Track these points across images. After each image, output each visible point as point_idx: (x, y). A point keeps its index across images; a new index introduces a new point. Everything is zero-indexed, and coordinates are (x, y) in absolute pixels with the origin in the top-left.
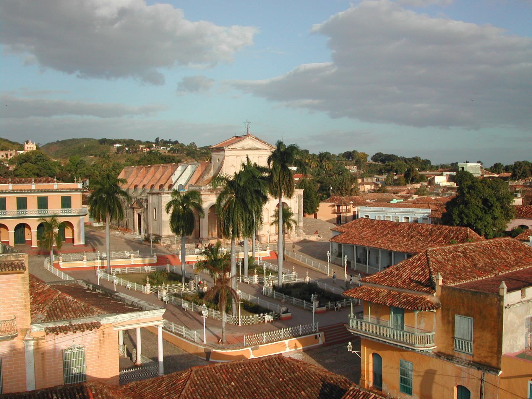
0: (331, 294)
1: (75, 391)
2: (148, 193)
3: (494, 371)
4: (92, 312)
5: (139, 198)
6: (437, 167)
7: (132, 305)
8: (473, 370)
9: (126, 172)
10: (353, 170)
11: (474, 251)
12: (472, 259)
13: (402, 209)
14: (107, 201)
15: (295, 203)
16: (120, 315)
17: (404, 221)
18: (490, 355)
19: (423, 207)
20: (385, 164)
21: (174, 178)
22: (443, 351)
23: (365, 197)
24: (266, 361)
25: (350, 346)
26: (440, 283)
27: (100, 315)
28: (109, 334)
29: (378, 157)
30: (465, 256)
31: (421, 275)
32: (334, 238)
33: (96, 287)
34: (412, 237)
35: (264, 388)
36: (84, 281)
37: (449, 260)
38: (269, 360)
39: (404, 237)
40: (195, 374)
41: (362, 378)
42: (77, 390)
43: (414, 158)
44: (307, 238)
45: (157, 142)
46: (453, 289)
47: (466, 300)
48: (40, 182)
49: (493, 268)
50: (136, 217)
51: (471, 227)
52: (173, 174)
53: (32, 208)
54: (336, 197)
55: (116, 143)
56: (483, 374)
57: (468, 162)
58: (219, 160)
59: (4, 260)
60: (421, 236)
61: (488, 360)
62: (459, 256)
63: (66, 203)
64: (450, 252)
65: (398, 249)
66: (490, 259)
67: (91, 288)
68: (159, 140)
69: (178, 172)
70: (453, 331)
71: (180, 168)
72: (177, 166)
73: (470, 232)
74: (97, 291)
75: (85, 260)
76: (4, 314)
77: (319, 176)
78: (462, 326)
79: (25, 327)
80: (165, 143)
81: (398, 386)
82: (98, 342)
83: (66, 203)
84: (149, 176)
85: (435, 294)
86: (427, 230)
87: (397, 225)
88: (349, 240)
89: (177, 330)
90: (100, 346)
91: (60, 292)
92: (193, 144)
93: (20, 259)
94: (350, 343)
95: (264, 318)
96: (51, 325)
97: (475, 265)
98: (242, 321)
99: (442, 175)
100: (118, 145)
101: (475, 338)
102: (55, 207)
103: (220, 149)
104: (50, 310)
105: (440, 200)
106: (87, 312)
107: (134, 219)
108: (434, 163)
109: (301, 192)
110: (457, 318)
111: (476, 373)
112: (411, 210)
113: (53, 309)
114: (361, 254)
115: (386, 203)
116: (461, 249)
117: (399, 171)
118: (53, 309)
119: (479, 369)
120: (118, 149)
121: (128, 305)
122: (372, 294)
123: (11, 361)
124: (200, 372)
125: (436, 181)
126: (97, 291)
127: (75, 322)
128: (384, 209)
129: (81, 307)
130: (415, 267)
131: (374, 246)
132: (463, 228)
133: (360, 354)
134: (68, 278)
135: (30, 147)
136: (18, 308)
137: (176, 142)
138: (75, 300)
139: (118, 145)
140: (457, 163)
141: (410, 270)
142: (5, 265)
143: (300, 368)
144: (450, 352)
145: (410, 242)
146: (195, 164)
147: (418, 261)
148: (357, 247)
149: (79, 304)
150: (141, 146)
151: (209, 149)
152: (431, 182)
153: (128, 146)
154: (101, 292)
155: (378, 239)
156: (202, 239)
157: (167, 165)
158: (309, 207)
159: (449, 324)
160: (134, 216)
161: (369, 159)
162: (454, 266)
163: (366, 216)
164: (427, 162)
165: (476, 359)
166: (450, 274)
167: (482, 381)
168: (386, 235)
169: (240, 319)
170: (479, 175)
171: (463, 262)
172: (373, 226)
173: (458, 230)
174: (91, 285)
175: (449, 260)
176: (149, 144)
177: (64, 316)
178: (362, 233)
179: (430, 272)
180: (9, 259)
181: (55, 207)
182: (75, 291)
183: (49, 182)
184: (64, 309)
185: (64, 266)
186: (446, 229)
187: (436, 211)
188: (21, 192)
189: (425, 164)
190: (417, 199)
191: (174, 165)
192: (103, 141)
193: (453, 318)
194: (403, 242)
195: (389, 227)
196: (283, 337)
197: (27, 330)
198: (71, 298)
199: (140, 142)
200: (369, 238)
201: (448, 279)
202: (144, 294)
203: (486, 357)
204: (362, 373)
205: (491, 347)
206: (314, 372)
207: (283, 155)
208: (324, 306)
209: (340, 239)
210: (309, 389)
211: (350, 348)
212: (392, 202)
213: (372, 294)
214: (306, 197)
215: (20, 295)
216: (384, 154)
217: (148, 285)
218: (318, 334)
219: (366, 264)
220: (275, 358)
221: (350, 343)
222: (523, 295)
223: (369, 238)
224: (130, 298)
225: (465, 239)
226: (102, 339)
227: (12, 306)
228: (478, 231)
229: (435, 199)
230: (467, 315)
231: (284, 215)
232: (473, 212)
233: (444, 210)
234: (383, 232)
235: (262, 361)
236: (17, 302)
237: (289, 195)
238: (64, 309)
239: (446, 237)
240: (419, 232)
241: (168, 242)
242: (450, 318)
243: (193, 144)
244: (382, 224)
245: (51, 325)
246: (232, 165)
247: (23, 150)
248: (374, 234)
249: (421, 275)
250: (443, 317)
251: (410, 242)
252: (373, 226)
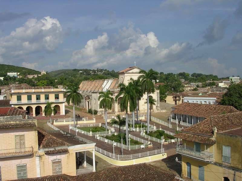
0: (170, 136)
1: (55, 178)
2: (92, 93)
3: (240, 170)
4: (64, 145)
5: (88, 94)
6: (220, 79)
7: (82, 141)
8: (231, 170)
9: (83, 83)
10: (183, 80)
11: (232, 117)
12: (231, 120)
13: (203, 98)
14: (74, 97)
15: (155, 96)
16: (76, 146)
17: (204, 103)
18: (238, 163)
19: (213, 97)
20: (197, 77)
21: (103, 86)
22: (218, 162)
23: (188, 93)
24: (138, 166)
25: (177, 159)
26: (216, 131)
27: (68, 146)
28: (72, 154)
29: (193, 75)
30: (228, 119)
31: (208, 128)
32: (172, 111)
33: (68, 133)
34: (207, 110)
35: (137, 178)
36: (63, 131)
37: (220, 121)
38: (140, 166)
39: (203, 110)
40: (107, 171)
41: (182, 173)
42: (56, 178)
43: (210, 75)
44: (161, 111)
45: (98, 70)
46: (222, 134)
47: (227, 139)
48: (46, 88)
49: (241, 125)
50: (87, 103)
51: (232, 105)
52: (103, 84)
53: (43, 99)
54: (174, 93)
55: (80, 71)
56: (235, 172)
57: (233, 76)
58: (122, 78)
59: (27, 122)
60: (211, 110)
61: (237, 166)
62: (226, 119)
63: (57, 97)
64: (221, 118)
65: (201, 116)
66: (239, 121)
67: (65, 134)
68: (99, 69)
69: (105, 83)
70: (222, 153)
71: (106, 81)
72: (105, 80)
73: (233, 108)
74: (68, 135)
75: (65, 121)
76: (27, 145)
77: (171, 84)
78: (226, 151)
79: (36, 151)
80: (101, 71)
81: (198, 176)
82: (67, 157)
83: (57, 97)
84: (93, 85)
85: (214, 136)
86: (213, 107)
87: (200, 105)
88: (179, 112)
89: (102, 152)
90: (68, 159)
91: (51, 136)
92: (113, 71)
93: (34, 122)
94: (177, 158)
95: (140, 147)
96: (47, 150)
97: (233, 123)
98: (130, 148)
99: (222, 82)
100: (81, 72)
101: (231, 156)
102: (52, 99)
103: (123, 73)
104: (47, 143)
105: (221, 94)
106: (62, 144)
107: (86, 104)
108: (219, 77)
109: (158, 91)
110: (224, 147)
111: (232, 172)
112: (207, 98)
113: (48, 143)
114: (184, 118)
115: (196, 95)
116: (226, 116)
117: (206, 81)
118: (48, 143)
119: (233, 170)
120: (81, 73)
121: (80, 141)
122: (186, 136)
123: (30, 165)
124: (109, 171)
125: (219, 85)
126: (68, 135)
127: (57, 149)
128: (195, 98)
129: (59, 142)
130: (205, 124)
131: (190, 115)
132: (230, 106)
133: (181, 163)
134: (57, 129)
135: (43, 73)
136: (33, 142)
137: (106, 70)
138: (57, 139)
139: (81, 72)
140: (229, 77)
141: (203, 126)
142: (27, 124)
143: (153, 169)
144: (221, 162)
145: (206, 113)
146: (112, 80)
147: (207, 121)
148: (182, 115)
149: (59, 141)
150: (91, 72)
151: (118, 73)
152: (217, 86)
153: (85, 72)
154: (69, 136)
155: (192, 111)
156: (115, 112)
157: (100, 80)
158: (162, 99)
159: (220, 150)
160: (86, 102)
161: (190, 76)
162: (223, 124)
163: (187, 101)
164: (216, 77)
165: (232, 165)
166: (221, 127)
167: (235, 175)
168: (195, 110)
169: (130, 147)
170: (239, 82)
171: (227, 122)
172: (190, 106)
173: (227, 107)
174: (65, 133)
175: (220, 121)
176: (94, 71)
177: (52, 146)
178: (185, 109)
179: (212, 126)
180: (29, 122)
181: (52, 99)
182: (58, 135)
183: (50, 88)
184: (53, 143)
185: (56, 125)
186: (222, 107)
187: (218, 98)
188: (38, 92)
189: (215, 78)
190: (211, 93)
191: (103, 80)
192: (75, 70)
193: (222, 148)
194: (203, 113)
195: (197, 106)
196: (148, 155)
197: (37, 152)
198: (55, 138)
199: (90, 70)
200: (188, 111)
201: (220, 130)
202: (90, 137)
203: (236, 164)
204: (182, 171)
205: (238, 160)
206: (160, 171)
207: (151, 75)
208: (167, 141)
209: (175, 112)
210: (157, 178)
211: (177, 160)
212: (199, 95)
213: (186, 136)
214: (161, 93)
215: (34, 137)
216: (197, 73)
217: (91, 132)
218: (164, 154)
219: (186, 122)
220: (143, 165)
221: (177, 158)
222: (22, 169)
223: (188, 111)
224: (81, 139)
225: (231, 111)
226: (68, 156)
227: (30, 142)
228: (236, 107)
229: (219, 93)
230: (228, 146)
231: (151, 101)
232: (234, 99)
233: (222, 98)
234: (194, 108)
235: (137, 166)
236: (33, 140)
237: (153, 91)
238: (53, 143)
239: (222, 110)
240: (210, 108)
241: (100, 114)
242: (221, 147)
243: (113, 71)
244: (194, 105)
245: (47, 150)
246: (126, 80)
247: (41, 74)
248: (190, 109)
249: (208, 128)
250: (217, 146)
251: (206, 113)
252: (190, 106)
